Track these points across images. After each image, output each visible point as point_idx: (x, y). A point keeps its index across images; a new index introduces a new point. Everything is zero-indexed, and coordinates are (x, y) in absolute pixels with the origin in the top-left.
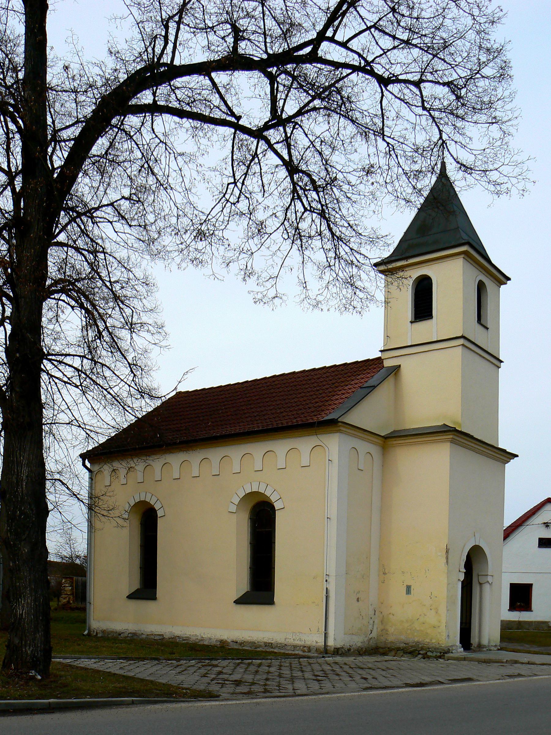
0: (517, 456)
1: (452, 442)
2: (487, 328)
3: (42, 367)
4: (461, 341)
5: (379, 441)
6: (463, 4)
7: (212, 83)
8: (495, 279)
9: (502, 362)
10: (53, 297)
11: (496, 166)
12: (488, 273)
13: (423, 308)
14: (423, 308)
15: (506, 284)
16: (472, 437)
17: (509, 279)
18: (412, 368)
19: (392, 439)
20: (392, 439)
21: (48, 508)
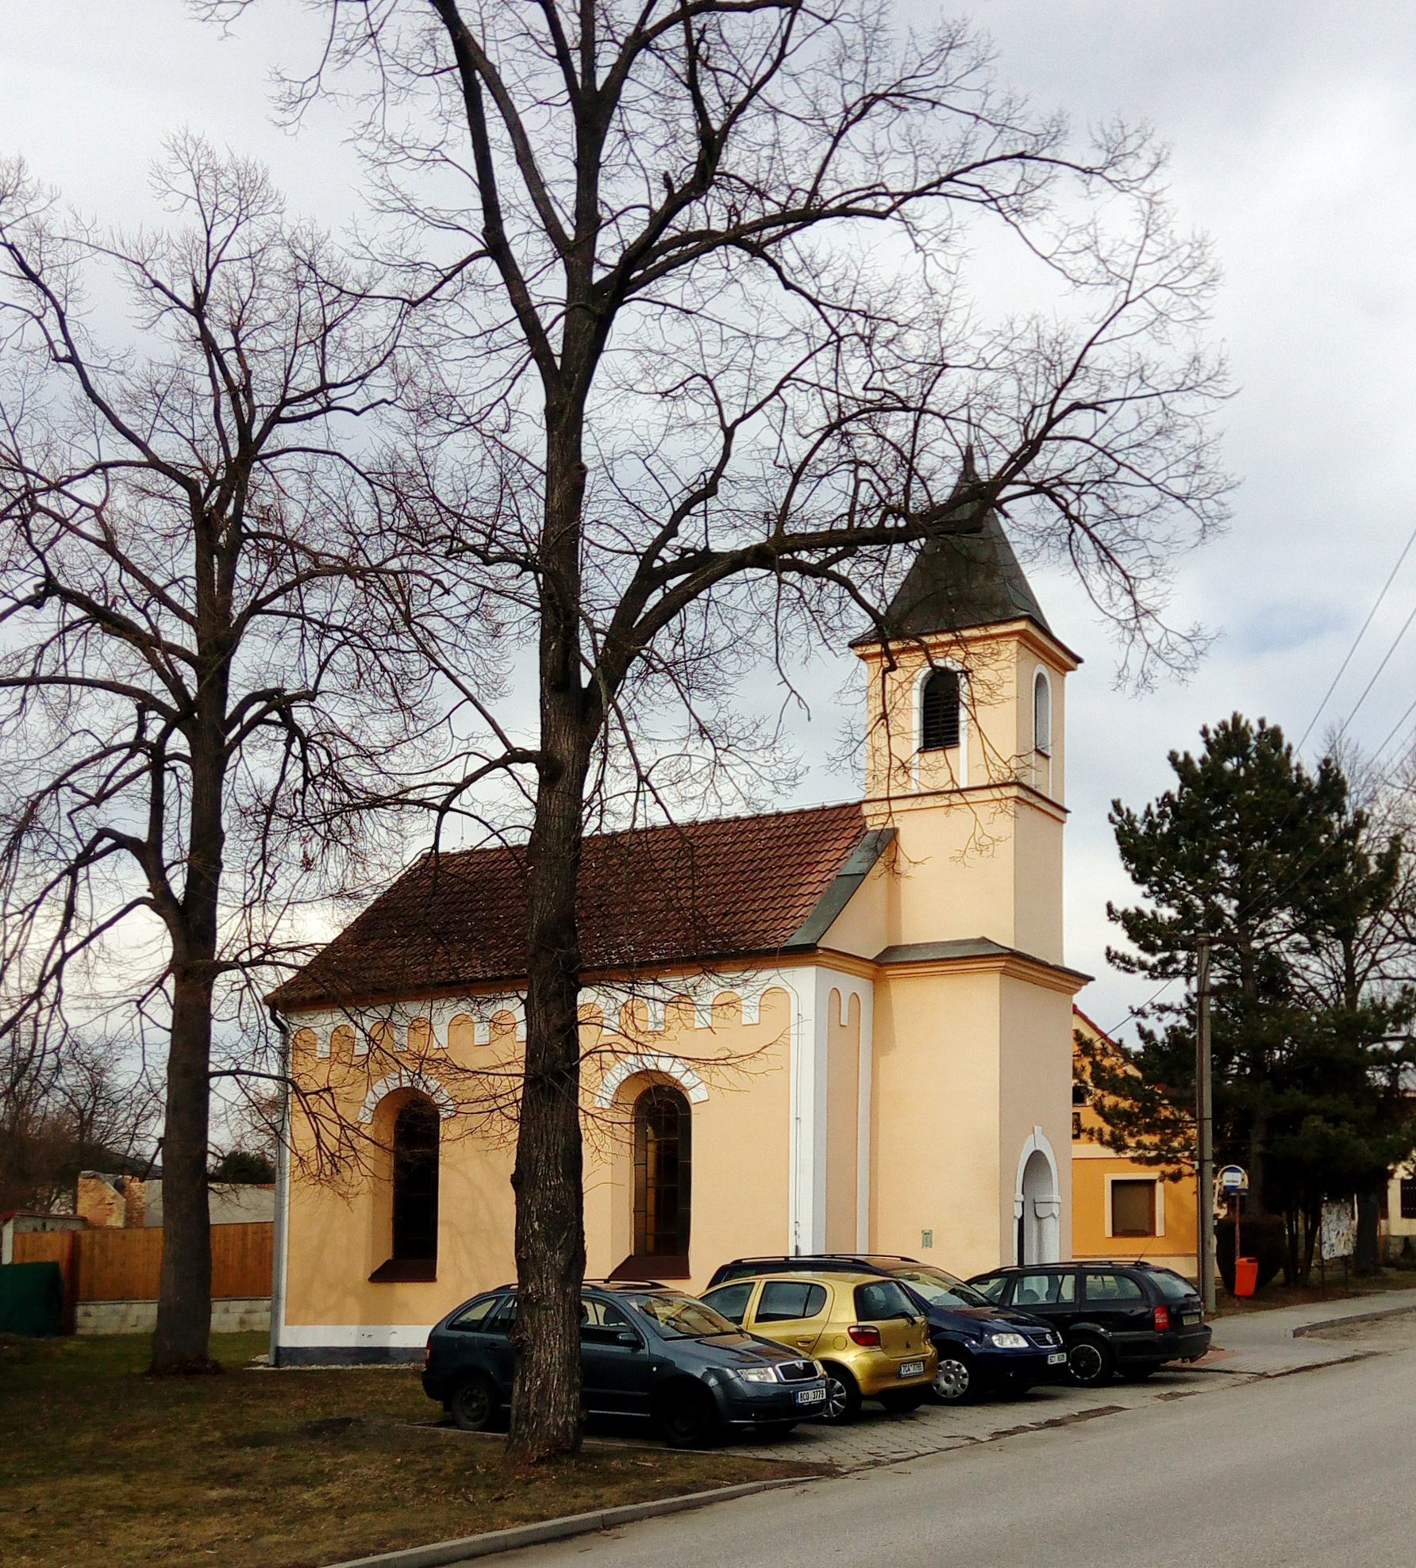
0: (1091, 979)
1: (1004, 972)
2: (1047, 757)
3: (244, 530)
4: (1014, 791)
5: (869, 970)
6: (6, 220)
7: (153, 790)
8: (1052, 659)
9: (1066, 811)
10: (203, 491)
11: (1201, 496)
12: (1056, 662)
13: (940, 729)
14: (940, 729)
15: (1073, 669)
16: (1034, 961)
17: (1079, 660)
18: (918, 834)
19: (889, 962)
20: (889, 962)
21: (207, 1062)
